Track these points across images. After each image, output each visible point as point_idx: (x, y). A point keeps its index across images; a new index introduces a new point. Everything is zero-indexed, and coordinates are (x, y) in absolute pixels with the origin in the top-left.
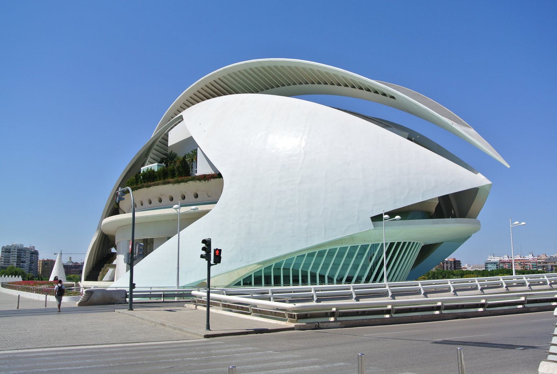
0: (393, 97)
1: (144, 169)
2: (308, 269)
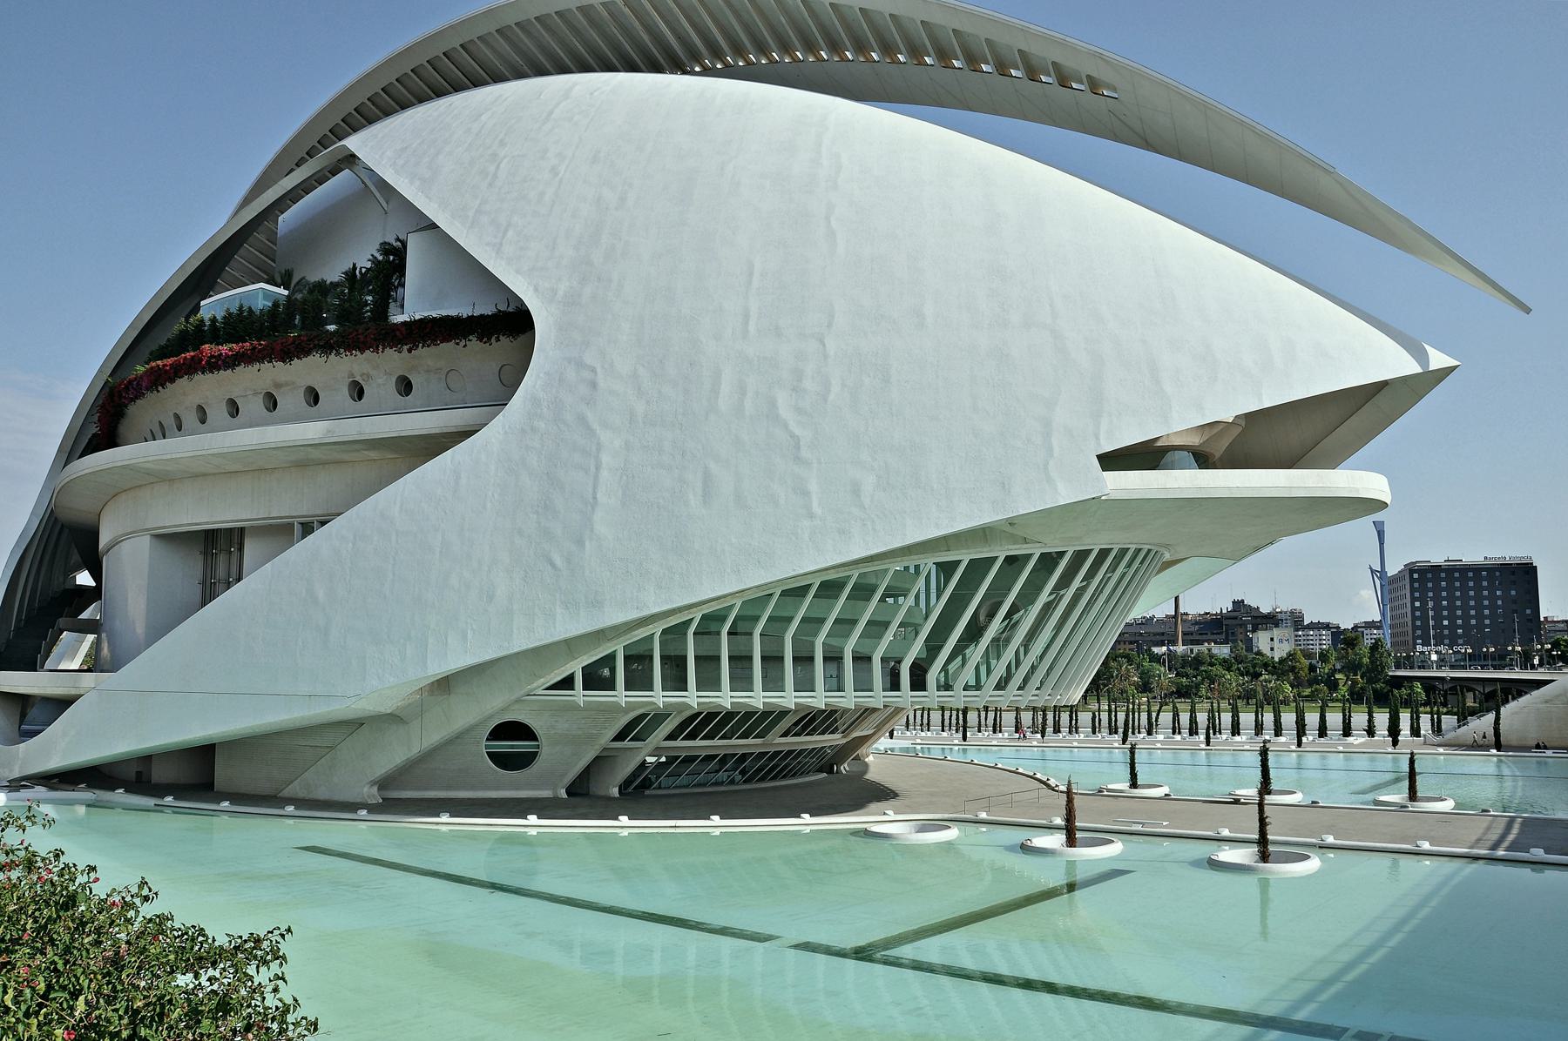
0: (1094, 85)
1: (213, 306)
2: (786, 630)
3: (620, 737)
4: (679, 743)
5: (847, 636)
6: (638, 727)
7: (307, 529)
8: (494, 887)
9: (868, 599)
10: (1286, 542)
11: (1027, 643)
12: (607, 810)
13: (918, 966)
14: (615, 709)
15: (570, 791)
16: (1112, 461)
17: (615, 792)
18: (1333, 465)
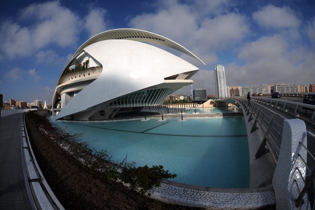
0: (163, 41)
1: (71, 68)
3: (113, 111)
4: (120, 112)
5: (137, 99)
6: (115, 110)
7: (80, 91)
8: (168, 135)
9: (139, 95)
10: (184, 87)
11: (161, 95)
12: (112, 119)
13: (148, 133)
14: (113, 108)
15: (109, 117)
16: (165, 79)
17: (113, 117)
18: (188, 79)
